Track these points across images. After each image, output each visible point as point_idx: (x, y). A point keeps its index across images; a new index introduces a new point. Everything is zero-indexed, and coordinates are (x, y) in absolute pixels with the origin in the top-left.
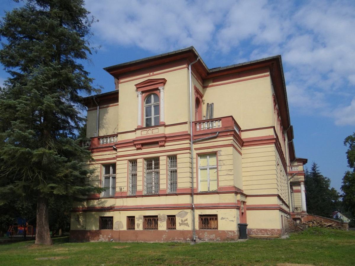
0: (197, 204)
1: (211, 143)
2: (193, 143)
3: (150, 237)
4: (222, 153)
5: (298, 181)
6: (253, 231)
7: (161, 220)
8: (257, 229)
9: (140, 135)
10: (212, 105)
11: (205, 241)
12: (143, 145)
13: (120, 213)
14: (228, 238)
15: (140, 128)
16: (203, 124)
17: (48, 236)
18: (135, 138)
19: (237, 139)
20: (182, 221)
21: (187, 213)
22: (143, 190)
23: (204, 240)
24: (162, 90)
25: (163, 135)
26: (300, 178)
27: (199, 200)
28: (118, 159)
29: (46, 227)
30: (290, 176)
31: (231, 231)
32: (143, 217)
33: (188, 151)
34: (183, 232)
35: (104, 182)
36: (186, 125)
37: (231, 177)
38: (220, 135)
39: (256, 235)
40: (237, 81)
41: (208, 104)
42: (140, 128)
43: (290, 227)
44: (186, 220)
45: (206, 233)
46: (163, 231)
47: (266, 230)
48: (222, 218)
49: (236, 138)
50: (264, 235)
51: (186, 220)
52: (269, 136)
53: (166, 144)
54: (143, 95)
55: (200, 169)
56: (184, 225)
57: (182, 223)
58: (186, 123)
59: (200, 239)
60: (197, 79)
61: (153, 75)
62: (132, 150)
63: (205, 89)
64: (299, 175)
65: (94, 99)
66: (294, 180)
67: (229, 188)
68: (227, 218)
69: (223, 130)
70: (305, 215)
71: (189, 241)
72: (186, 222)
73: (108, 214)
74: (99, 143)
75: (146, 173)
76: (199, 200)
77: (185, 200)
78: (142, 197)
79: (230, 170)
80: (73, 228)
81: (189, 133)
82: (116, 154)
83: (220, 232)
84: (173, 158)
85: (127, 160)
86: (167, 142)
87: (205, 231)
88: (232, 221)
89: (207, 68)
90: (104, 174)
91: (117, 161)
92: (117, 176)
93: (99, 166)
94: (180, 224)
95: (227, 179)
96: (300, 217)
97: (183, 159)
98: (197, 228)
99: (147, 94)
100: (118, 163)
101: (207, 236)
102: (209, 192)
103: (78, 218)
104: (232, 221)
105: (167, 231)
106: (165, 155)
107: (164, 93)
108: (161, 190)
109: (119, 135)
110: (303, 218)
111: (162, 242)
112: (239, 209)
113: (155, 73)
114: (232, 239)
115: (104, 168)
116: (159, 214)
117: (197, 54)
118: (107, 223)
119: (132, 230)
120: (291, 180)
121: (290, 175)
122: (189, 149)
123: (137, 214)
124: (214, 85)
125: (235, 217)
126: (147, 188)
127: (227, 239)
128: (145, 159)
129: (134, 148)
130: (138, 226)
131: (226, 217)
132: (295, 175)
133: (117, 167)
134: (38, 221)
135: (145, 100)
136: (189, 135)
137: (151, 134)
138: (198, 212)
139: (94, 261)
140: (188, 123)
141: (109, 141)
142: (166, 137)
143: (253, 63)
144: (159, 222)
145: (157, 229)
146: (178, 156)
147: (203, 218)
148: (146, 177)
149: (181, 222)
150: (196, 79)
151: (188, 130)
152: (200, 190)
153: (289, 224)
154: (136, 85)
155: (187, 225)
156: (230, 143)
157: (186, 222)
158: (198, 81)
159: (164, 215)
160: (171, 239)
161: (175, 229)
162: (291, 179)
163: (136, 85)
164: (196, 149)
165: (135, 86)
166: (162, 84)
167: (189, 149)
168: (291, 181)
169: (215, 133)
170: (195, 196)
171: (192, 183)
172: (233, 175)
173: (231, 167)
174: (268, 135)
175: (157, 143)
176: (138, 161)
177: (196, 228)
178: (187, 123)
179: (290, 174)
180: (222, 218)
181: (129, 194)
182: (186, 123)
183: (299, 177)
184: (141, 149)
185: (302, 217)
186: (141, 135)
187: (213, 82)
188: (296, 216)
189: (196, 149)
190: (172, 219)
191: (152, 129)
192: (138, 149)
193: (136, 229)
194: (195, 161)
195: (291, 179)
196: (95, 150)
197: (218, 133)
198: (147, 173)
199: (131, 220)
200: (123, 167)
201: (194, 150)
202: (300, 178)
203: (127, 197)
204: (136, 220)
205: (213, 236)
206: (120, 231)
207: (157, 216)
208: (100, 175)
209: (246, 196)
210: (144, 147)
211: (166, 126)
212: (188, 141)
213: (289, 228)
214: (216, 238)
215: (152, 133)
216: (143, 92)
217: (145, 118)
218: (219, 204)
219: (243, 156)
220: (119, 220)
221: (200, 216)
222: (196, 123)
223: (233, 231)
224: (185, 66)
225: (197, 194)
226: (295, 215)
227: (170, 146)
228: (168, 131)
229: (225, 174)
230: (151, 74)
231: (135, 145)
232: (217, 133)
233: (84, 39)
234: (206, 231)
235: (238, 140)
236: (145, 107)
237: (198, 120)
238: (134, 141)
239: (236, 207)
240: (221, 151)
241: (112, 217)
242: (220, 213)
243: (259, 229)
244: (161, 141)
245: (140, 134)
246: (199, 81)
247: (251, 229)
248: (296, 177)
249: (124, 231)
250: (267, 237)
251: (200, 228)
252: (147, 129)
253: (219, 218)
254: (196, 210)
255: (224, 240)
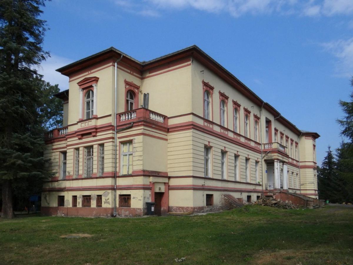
0: (119, 186)
1: (127, 133)
2: (117, 132)
3: (85, 213)
4: (135, 141)
5: (272, 158)
6: (174, 208)
7: (93, 199)
8: (176, 207)
9: (80, 127)
10: (148, 95)
11: (121, 217)
12: (83, 135)
13: (68, 193)
14: (136, 214)
15: (81, 121)
16: (122, 116)
17: (10, 212)
18: (77, 130)
19: (154, 128)
20: (106, 199)
21: (109, 193)
22: (83, 174)
23: (122, 216)
24: (95, 87)
25: (94, 127)
26: (273, 156)
27: (121, 182)
28: (68, 148)
29: (9, 205)
30: (264, 154)
31: (139, 209)
32: (82, 197)
33: (111, 140)
34: (106, 209)
35: (63, 167)
36: (110, 117)
37: (141, 162)
38: (134, 125)
39: (176, 212)
40: (185, 65)
41: (145, 94)
42: (81, 121)
43: (226, 205)
44: (108, 199)
45: (123, 210)
46: (94, 208)
47: (183, 208)
48: (134, 198)
49: (153, 127)
50: (181, 212)
51: (108, 199)
52: (189, 122)
53: (98, 134)
54: (84, 91)
55: (122, 156)
56: (107, 203)
57: (106, 202)
58: (110, 115)
59: (119, 215)
60: (132, 73)
61: (91, 73)
62: (74, 140)
63: (143, 80)
64: (273, 153)
65: (65, 94)
66: (268, 158)
67: (139, 171)
68: (137, 198)
69: (137, 120)
70: (277, 192)
71: (109, 216)
72: (108, 201)
73: (62, 194)
74: (59, 134)
75: (87, 159)
76: (121, 182)
77: (108, 182)
78: (82, 180)
79: (140, 156)
80: (43, 205)
81: (112, 124)
82: (67, 143)
83: (132, 209)
84: (102, 145)
85: (73, 148)
86: (98, 132)
87: (122, 209)
88: (140, 200)
89: (139, 61)
90: (63, 160)
91: (67, 149)
92: (68, 162)
93: (58, 153)
94: (105, 203)
95: (139, 164)
96: (272, 194)
97: (108, 146)
98: (118, 206)
99: (87, 90)
100: (68, 151)
101: (124, 213)
102: (128, 175)
103: (46, 197)
104: (140, 200)
105: (96, 208)
106: (97, 144)
107: (97, 89)
108: (94, 174)
109: (69, 127)
110: (275, 195)
111: (93, 217)
112: (151, 189)
113: (92, 71)
114: (140, 216)
115: (63, 155)
116: (92, 194)
117: (120, 53)
118: (61, 200)
119: (99, 207)
120: (265, 158)
121: (264, 153)
122: (113, 138)
123: (79, 194)
124: (149, 76)
125: (142, 197)
126: (87, 172)
127: (136, 215)
128: (85, 147)
129: (77, 138)
130: (79, 203)
131: (136, 197)
132: (269, 152)
133: (68, 154)
134: (3, 200)
135: (85, 96)
136: (113, 126)
137: (87, 126)
138: (119, 192)
139: (51, 230)
140: (112, 115)
141: (65, 132)
142: (96, 129)
143: (175, 54)
144: (92, 201)
145: (90, 206)
146: (105, 145)
147: (123, 197)
148: (87, 162)
149: (105, 201)
150: (130, 73)
151: (111, 122)
152: (121, 174)
153: (225, 202)
154: (78, 83)
155: (108, 203)
156: (141, 132)
157: (108, 201)
158: (132, 75)
159: (94, 194)
160: (98, 215)
161: (101, 206)
162: (265, 157)
163: (78, 83)
164: (119, 138)
165: (77, 84)
166: (95, 82)
167: (113, 138)
168: (265, 159)
169: (130, 123)
170: (118, 179)
171: (116, 167)
172: (142, 161)
173: (141, 153)
174: (188, 121)
175: (90, 133)
176: (94, 147)
177: (117, 206)
178: (111, 116)
179: (264, 152)
180: (134, 198)
181: (74, 177)
182: (110, 115)
183: (273, 154)
184: (82, 139)
185: (274, 194)
186: (81, 127)
187: (150, 73)
188: (268, 194)
189: (119, 138)
190: (99, 197)
191: (88, 122)
192: (80, 139)
193: (78, 206)
194: (118, 148)
195: (264, 156)
196: (55, 140)
197: (132, 123)
198: (88, 159)
199: (75, 198)
200: (70, 153)
201: (117, 139)
202: (273, 156)
203: (73, 180)
204: (78, 199)
205: (127, 213)
206: (68, 208)
207: (90, 196)
208: (58, 161)
209: (169, 178)
210: (84, 137)
211: (97, 118)
212: (111, 132)
213: (225, 206)
214: (129, 214)
215: (88, 125)
216: (83, 89)
217: (86, 111)
218: (132, 185)
219: (169, 141)
220: (67, 199)
221: (121, 196)
222: (120, 114)
223: (140, 209)
224: (111, 64)
225: (119, 177)
226: (267, 193)
227: (101, 135)
228: (100, 123)
229: (137, 160)
230: (90, 72)
231: (78, 135)
232: (131, 123)
233: (40, 46)
234: (124, 209)
235: (156, 128)
236: (86, 103)
237: (135, 109)
238: (76, 132)
239: (142, 188)
240: (135, 139)
241: (130, 195)
242: (133, 193)
243: (178, 207)
244: (93, 132)
245: (80, 126)
246: (134, 74)
247: (172, 207)
248: (269, 154)
249: (70, 208)
250: (181, 214)
251: (120, 206)
252: (84, 122)
253: (132, 197)
254: (117, 191)
255: (134, 216)
